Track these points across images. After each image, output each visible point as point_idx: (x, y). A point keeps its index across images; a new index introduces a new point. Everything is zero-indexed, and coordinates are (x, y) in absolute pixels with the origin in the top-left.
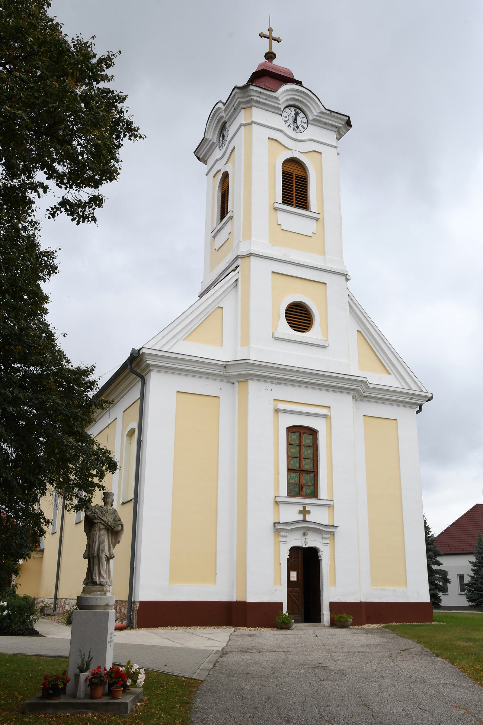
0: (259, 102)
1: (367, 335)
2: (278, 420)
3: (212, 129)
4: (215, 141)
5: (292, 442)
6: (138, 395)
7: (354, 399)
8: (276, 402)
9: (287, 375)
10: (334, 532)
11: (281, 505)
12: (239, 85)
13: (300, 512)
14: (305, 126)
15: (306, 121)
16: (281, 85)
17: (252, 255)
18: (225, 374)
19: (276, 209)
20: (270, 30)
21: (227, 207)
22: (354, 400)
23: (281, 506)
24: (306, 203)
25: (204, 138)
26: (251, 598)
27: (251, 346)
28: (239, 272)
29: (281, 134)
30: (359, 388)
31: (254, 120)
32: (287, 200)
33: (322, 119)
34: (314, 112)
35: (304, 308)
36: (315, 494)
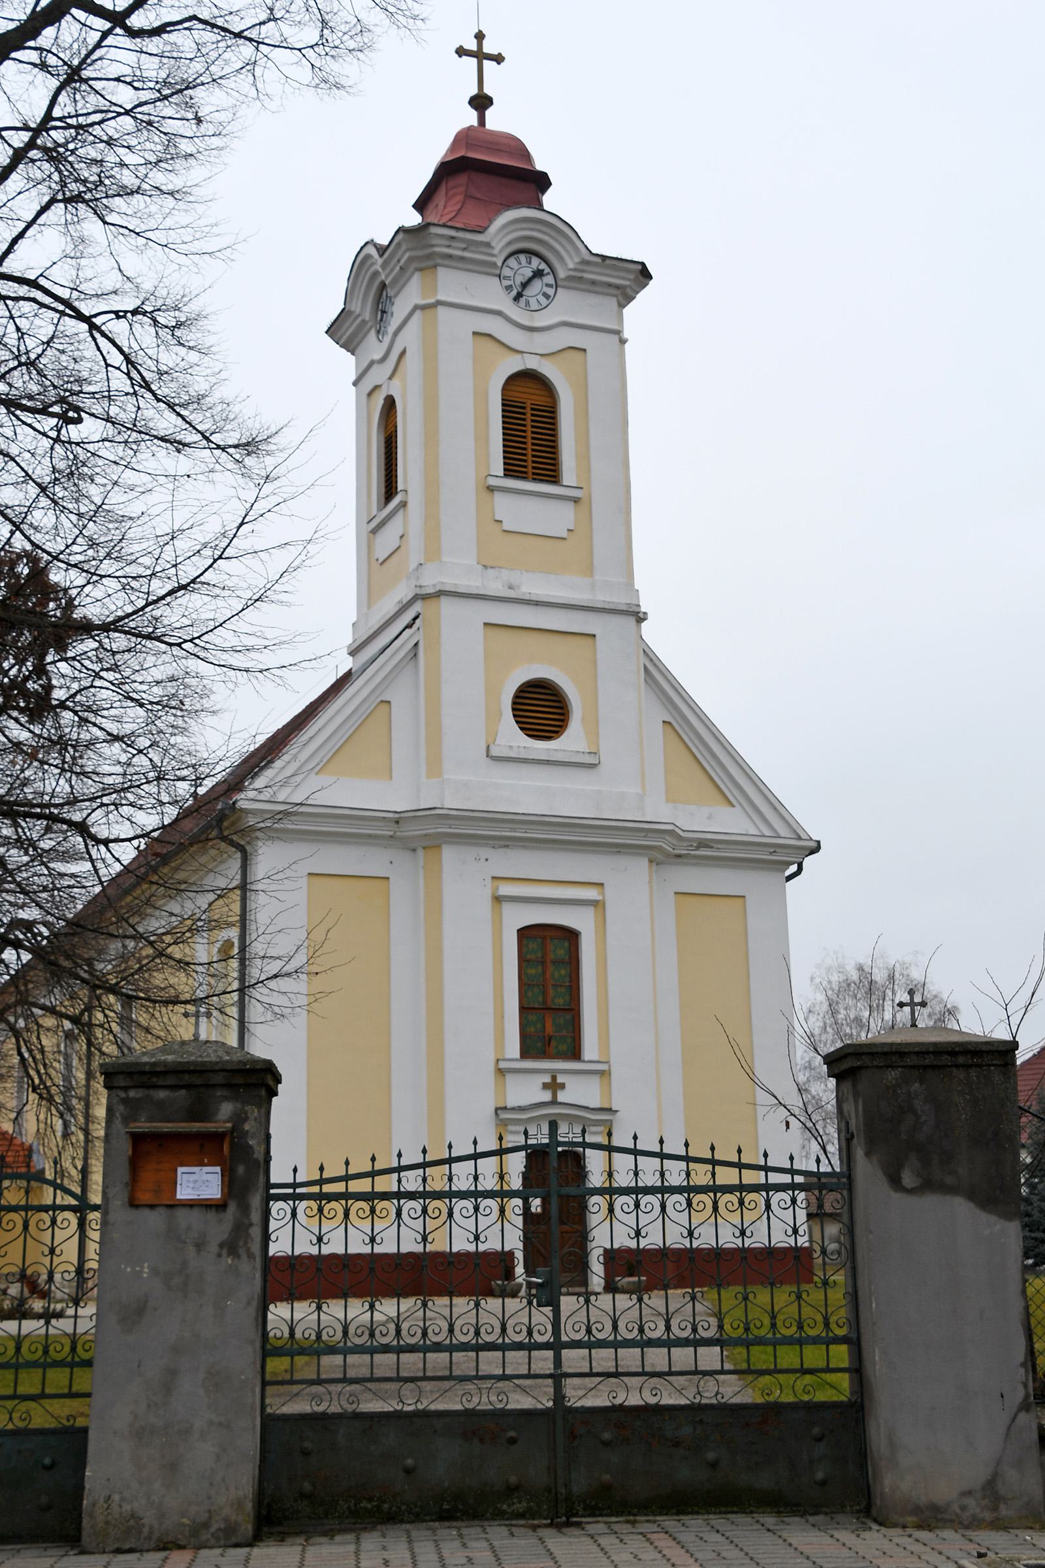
0: (450, 257)
1: (683, 730)
2: (501, 915)
4: (367, 318)
5: (529, 956)
8: (497, 883)
9: (514, 830)
10: (611, 1121)
12: (407, 225)
13: (545, 1086)
14: (551, 291)
15: (553, 283)
16: (498, 213)
18: (398, 834)
19: (491, 489)
20: (480, 36)
22: (654, 864)
23: (509, 1077)
25: (343, 310)
27: (446, 776)
29: (499, 321)
31: (441, 297)
33: (586, 275)
34: (566, 265)
36: (575, 1053)
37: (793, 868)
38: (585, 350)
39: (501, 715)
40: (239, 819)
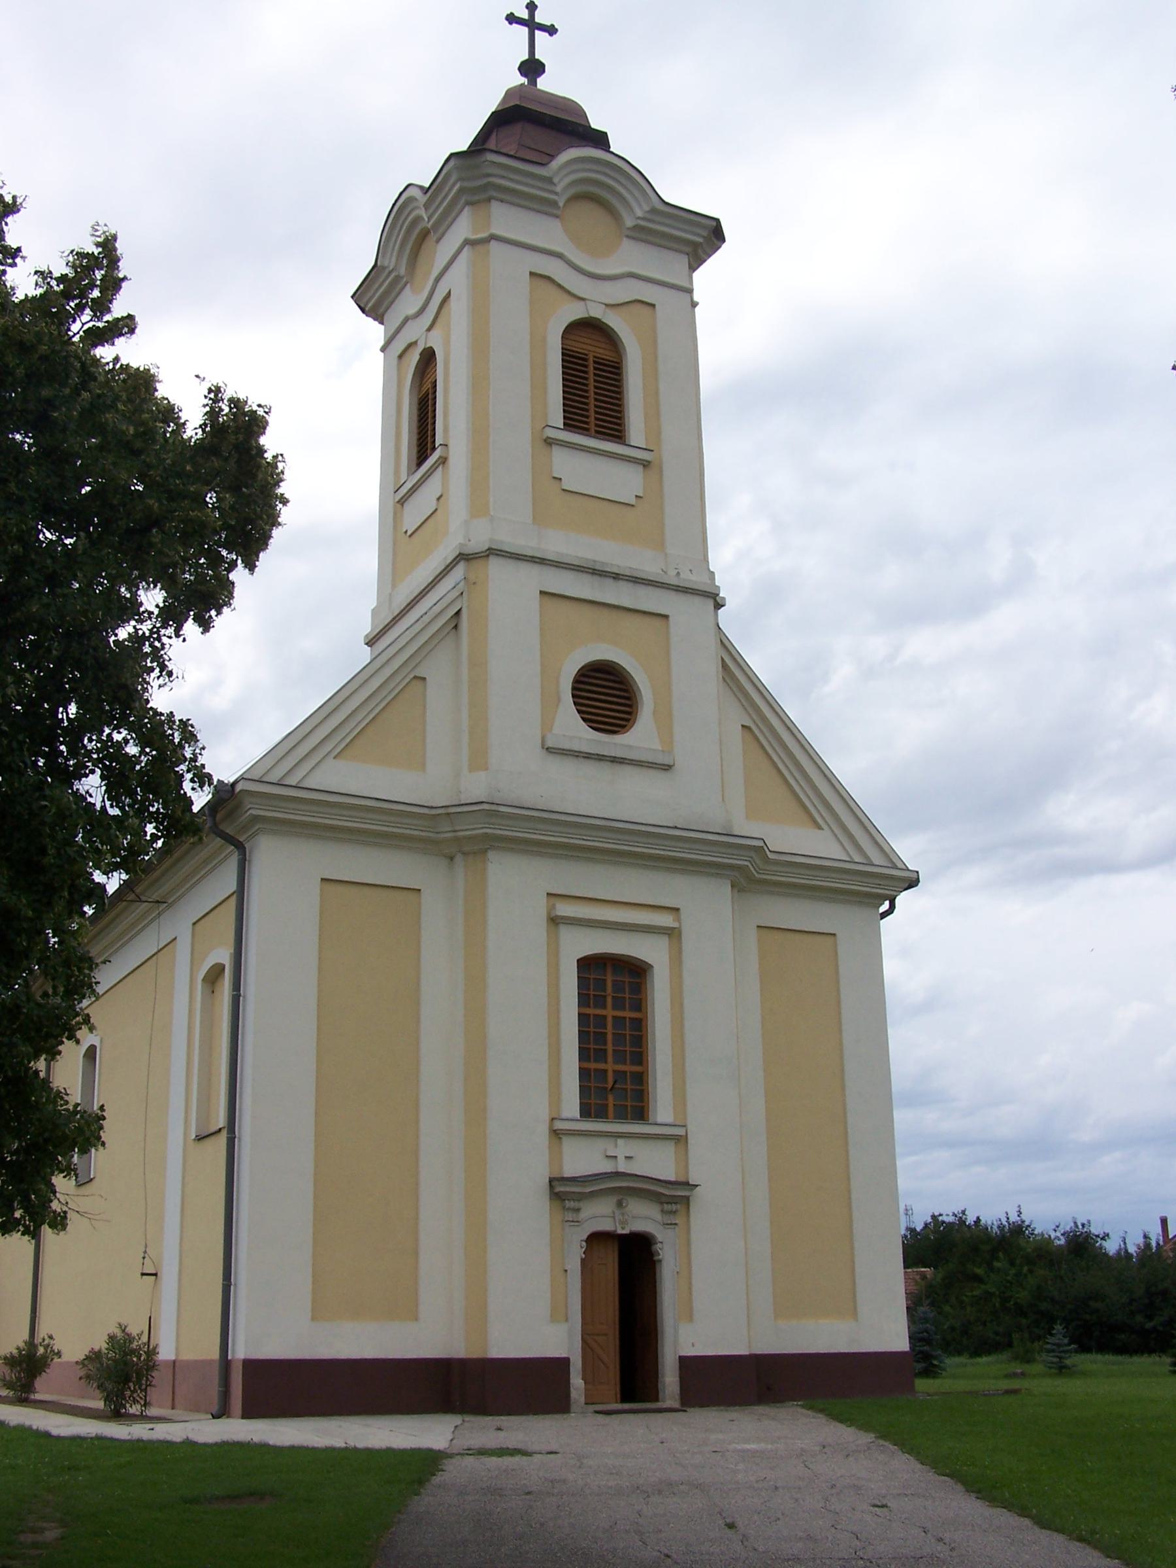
3: (392, 253)
6: (233, 886)
7: (736, 891)
8: (553, 900)
10: (687, 1198)
11: (565, 1139)
17: (492, 554)
19: (549, 442)
20: (531, 7)
21: (432, 421)
23: (567, 1142)
24: (620, 412)
26: (498, 1351)
28: (462, 593)
30: (746, 863)
32: (574, 419)
35: (618, 677)
36: (640, 1113)
37: (886, 906)
38: (653, 306)
39: (559, 700)
40: (238, 806)
